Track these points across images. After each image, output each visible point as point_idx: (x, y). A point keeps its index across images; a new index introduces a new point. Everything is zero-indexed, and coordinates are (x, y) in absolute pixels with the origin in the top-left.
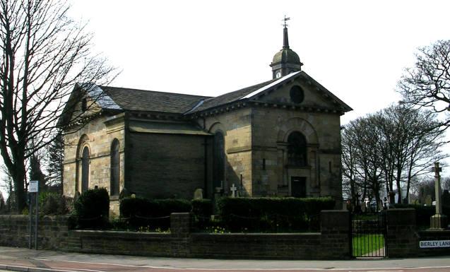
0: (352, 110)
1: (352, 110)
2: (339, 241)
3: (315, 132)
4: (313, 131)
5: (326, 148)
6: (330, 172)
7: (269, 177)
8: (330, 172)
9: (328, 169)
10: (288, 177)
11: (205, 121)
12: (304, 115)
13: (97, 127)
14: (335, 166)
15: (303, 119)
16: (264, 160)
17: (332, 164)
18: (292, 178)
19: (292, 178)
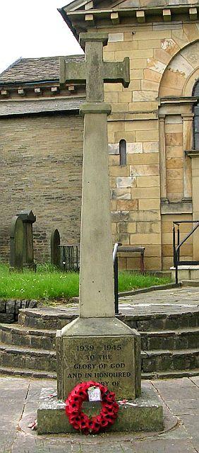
16: (123, 143)
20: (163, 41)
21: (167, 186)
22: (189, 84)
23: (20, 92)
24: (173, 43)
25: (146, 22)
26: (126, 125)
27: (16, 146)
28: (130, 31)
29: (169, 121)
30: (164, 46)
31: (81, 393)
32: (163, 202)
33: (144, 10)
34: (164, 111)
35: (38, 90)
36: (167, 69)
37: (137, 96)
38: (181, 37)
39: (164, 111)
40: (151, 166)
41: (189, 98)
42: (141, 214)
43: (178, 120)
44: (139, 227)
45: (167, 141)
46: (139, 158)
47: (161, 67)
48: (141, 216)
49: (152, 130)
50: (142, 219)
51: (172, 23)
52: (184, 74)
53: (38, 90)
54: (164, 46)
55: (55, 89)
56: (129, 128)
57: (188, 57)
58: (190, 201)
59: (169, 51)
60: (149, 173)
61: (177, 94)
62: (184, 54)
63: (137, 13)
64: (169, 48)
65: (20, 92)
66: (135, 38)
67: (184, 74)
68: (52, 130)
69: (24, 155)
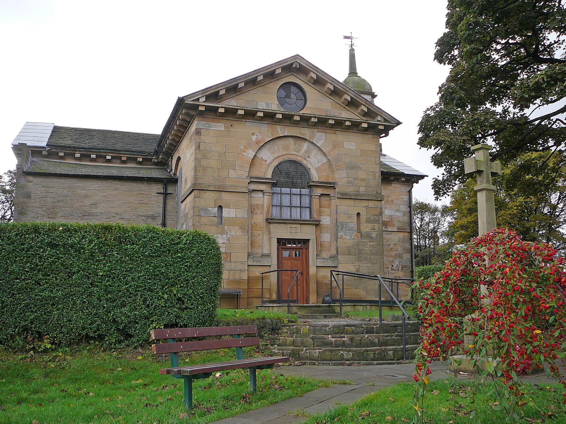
0: (399, 123)
1: (399, 123)
2: (74, 215)
3: (329, 160)
4: (325, 160)
5: (350, 190)
6: (359, 231)
7: (228, 240)
8: (359, 231)
9: (354, 225)
10: (270, 239)
11: (341, 306)
12: (306, 132)
13: (257, 322)
14: (368, 221)
15: (305, 139)
16: (220, 207)
17: (363, 217)
18: (279, 241)
19: (279, 241)
20: (253, 134)
21: (251, 244)
22: (269, 169)
23: (78, 155)
24: (260, 137)
25: (242, 118)
26: (223, 193)
27: (88, 202)
28: (229, 123)
29: (254, 195)
30: (254, 138)
31: (527, 319)
32: (249, 255)
33: (368, 123)
34: (253, 187)
35: (141, 160)
36: (255, 156)
37: (233, 174)
38: (266, 133)
39: (253, 187)
40: (242, 228)
41: (271, 179)
42: (233, 265)
43: (260, 195)
44: (231, 274)
45: (252, 210)
46: (233, 221)
47: (251, 154)
48: (233, 266)
49: (243, 200)
50: (233, 268)
51: (262, 122)
52: (266, 161)
53: (94, 156)
54: (254, 138)
55: (141, 160)
56: (225, 197)
57: (270, 149)
58: (268, 256)
59: (257, 143)
60: (239, 233)
61: (262, 175)
62: (267, 146)
63: (277, 115)
64: (258, 140)
65: (78, 155)
66: (232, 129)
67: (266, 161)
68: (121, 192)
69: (94, 210)
